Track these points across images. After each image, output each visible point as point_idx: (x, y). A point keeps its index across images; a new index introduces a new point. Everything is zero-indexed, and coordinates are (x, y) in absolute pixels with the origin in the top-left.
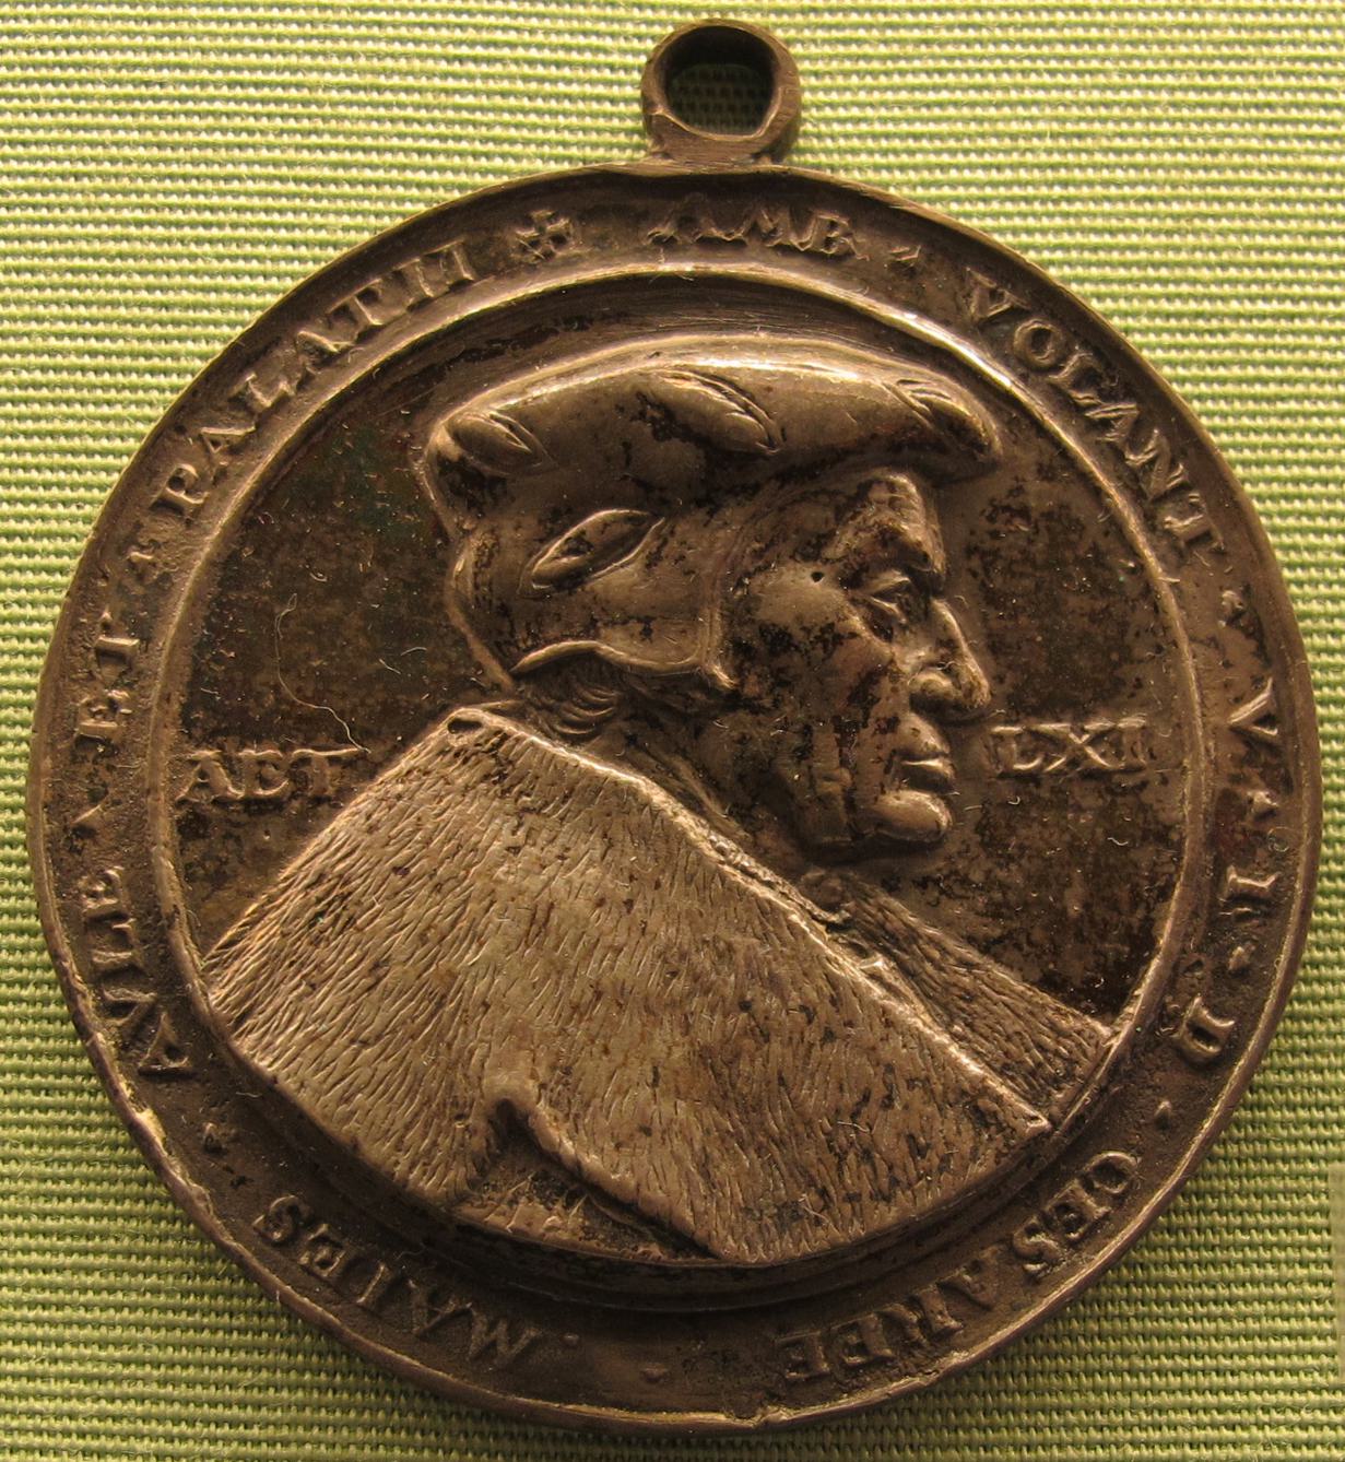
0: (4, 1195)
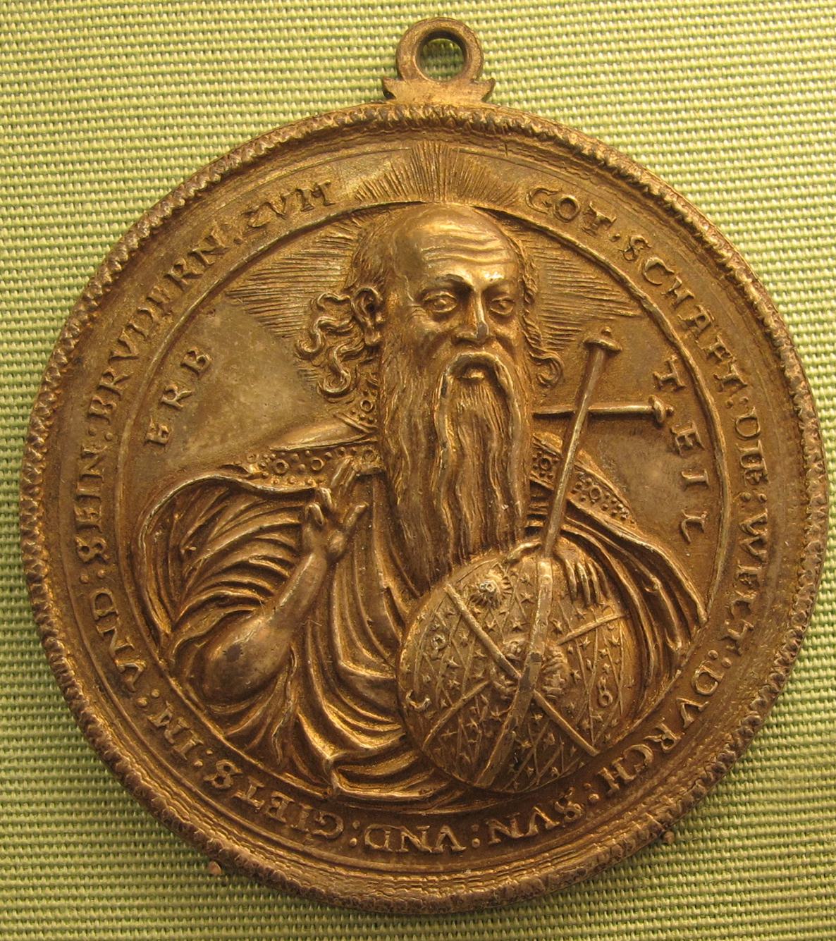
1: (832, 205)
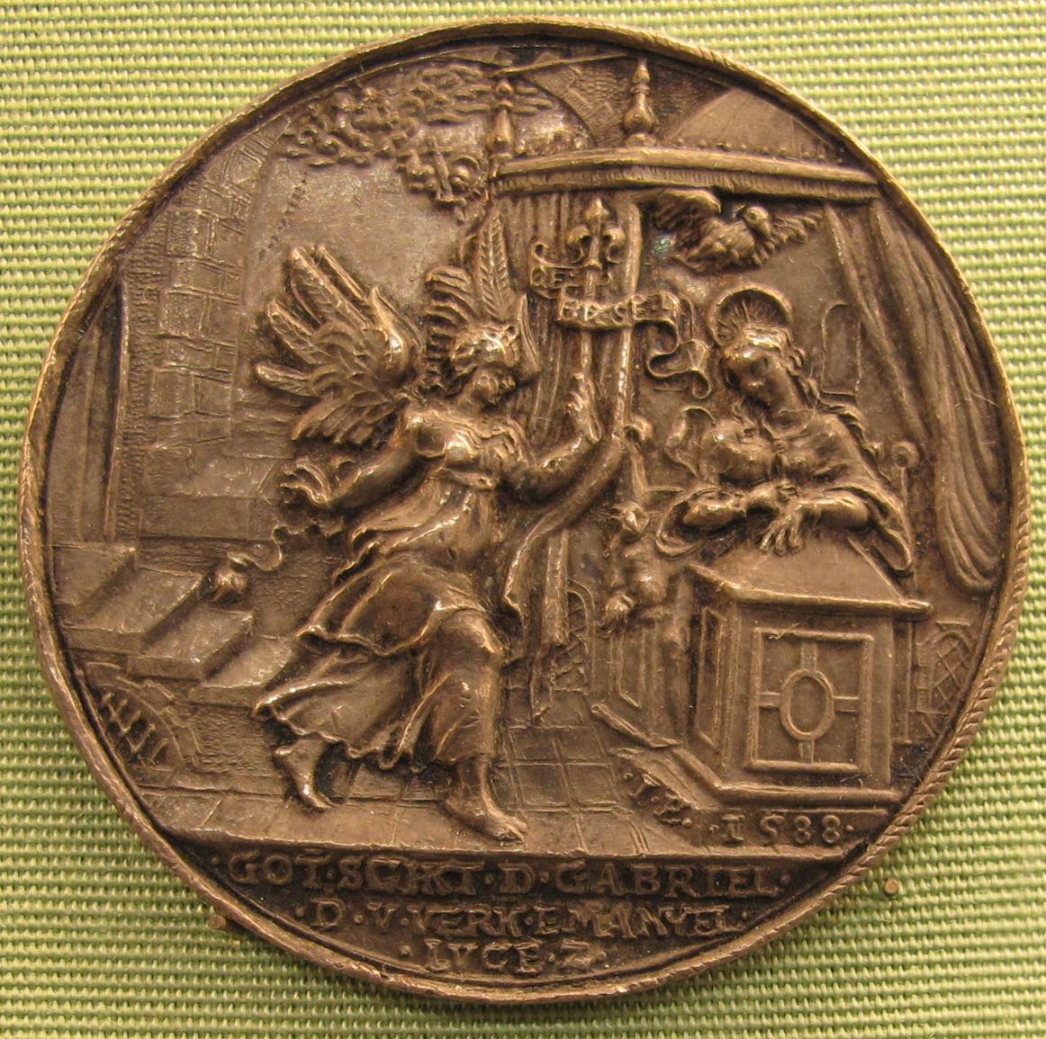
1: (1041, 989)
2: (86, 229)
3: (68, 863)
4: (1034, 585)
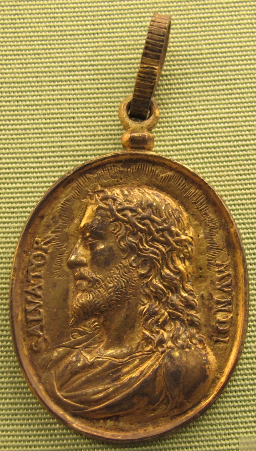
0: (1, 130)
2: (10, 124)
3: (10, 396)
4: (252, 321)
